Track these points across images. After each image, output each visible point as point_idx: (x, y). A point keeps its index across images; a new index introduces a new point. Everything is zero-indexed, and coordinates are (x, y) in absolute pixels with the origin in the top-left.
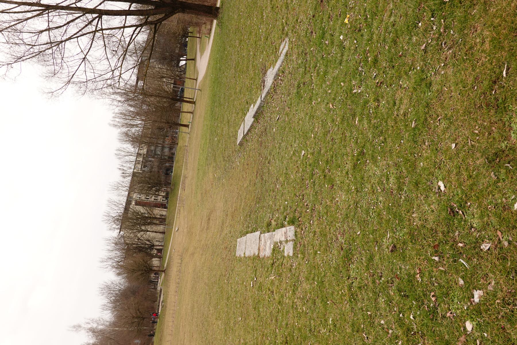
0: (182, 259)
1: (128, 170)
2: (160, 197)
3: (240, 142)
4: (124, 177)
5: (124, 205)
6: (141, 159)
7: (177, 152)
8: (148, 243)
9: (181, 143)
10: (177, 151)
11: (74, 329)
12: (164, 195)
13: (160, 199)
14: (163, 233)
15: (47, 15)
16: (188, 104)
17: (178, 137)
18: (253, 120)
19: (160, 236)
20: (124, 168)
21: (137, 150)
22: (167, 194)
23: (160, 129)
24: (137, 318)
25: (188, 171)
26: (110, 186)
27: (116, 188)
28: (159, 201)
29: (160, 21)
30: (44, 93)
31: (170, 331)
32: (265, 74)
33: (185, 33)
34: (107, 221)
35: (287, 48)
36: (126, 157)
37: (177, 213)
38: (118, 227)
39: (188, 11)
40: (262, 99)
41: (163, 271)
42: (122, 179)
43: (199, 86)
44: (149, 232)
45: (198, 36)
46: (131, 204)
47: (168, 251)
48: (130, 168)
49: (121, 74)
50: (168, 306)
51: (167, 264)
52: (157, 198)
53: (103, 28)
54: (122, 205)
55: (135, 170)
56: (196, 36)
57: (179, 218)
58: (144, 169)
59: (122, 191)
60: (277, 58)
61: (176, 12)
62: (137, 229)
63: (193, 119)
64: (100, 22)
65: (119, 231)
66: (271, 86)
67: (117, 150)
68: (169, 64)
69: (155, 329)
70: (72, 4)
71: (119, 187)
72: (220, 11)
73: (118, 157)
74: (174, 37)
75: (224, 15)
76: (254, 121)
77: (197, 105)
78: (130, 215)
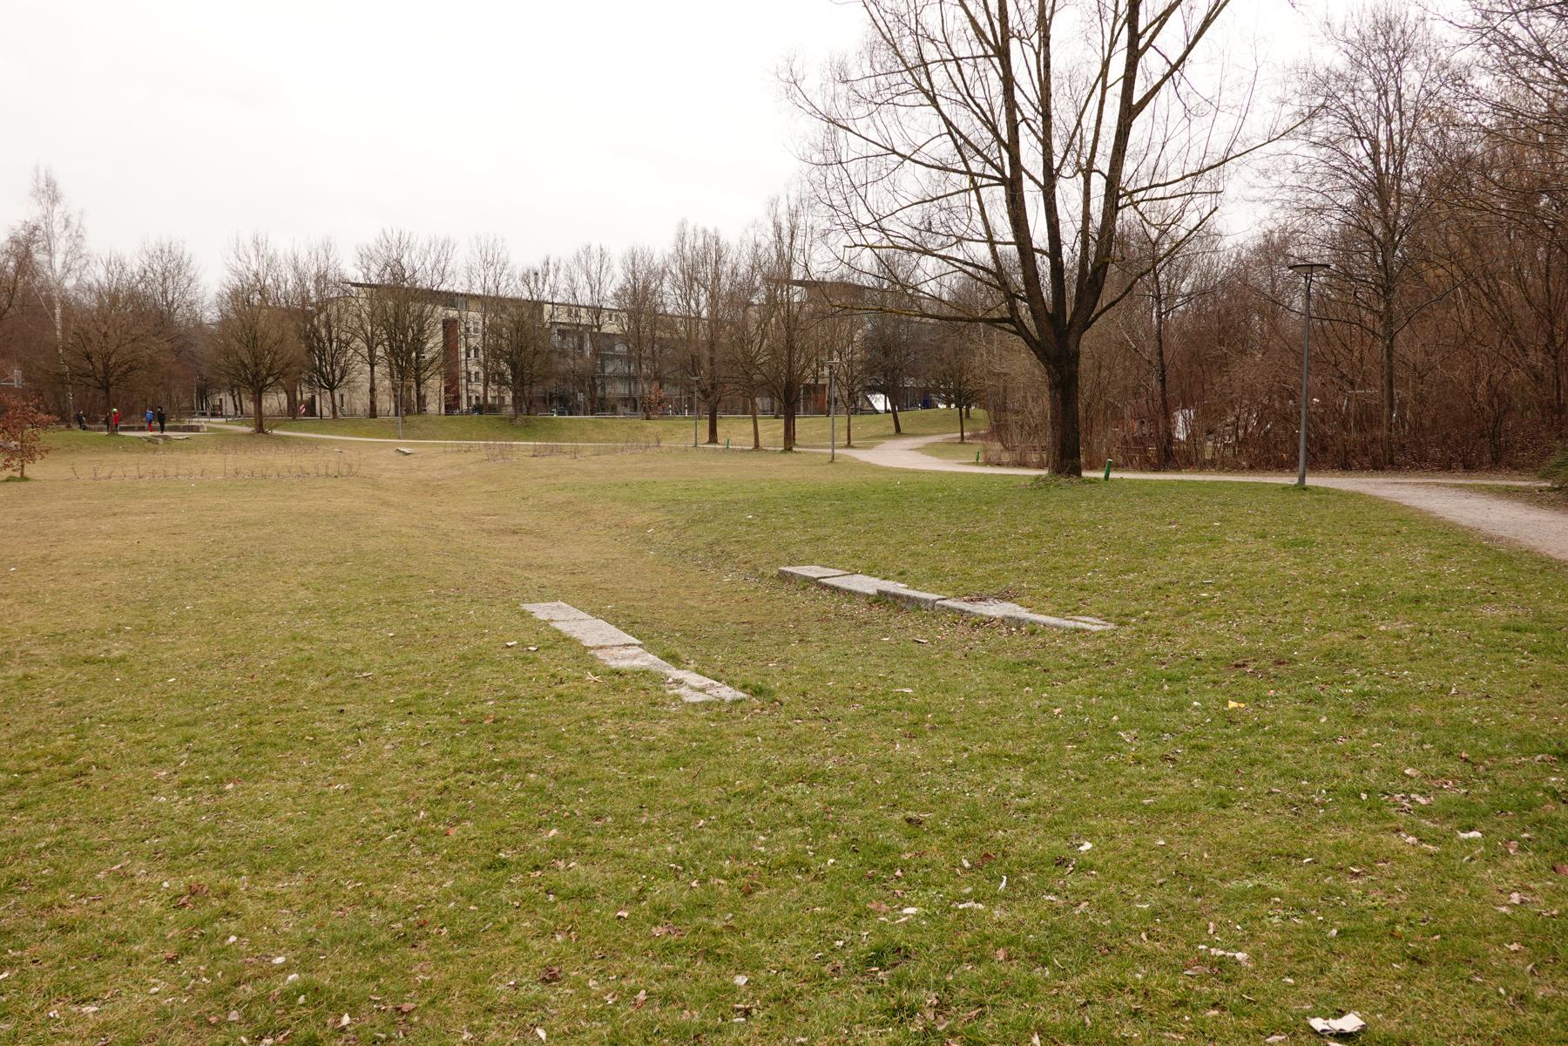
0: (342, 476)
3: (792, 574)
4: (525, 279)
5: (443, 288)
6: (585, 319)
7: (624, 421)
9: (655, 426)
10: (630, 421)
11: (42, 185)
12: (490, 400)
14: (373, 413)
15: (981, 52)
16: (782, 430)
17: (667, 419)
19: (361, 401)
22: (492, 409)
24: (106, 366)
25: (594, 458)
26: (491, 241)
27: (489, 259)
29: (1021, 330)
30: (790, 61)
31: (106, 474)
32: (1003, 599)
33: (968, 398)
34: (385, 243)
35: (1095, 628)
36: (585, 278)
37: (458, 445)
38: (373, 279)
39: (1058, 396)
40: (938, 602)
42: (518, 273)
43: (840, 455)
45: (965, 434)
47: (323, 434)
48: (554, 294)
49: (871, 247)
50: (160, 456)
51: (286, 436)
52: (473, 380)
53: (981, 190)
54: (439, 281)
55: (548, 308)
56: (965, 429)
59: (482, 277)
60: (1061, 611)
61: (1051, 367)
62: (372, 333)
63: (743, 451)
64: (996, 182)
65: (361, 280)
66: (981, 615)
67: (602, 249)
68: (870, 367)
69: (69, 427)
70: (1022, 115)
71: (492, 268)
72: (1074, 479)
73: (581, 253)
74: (952, 369)
75: (1067, 489)
76: (868, 596)
77: (960, 446)
78: (414, 307)
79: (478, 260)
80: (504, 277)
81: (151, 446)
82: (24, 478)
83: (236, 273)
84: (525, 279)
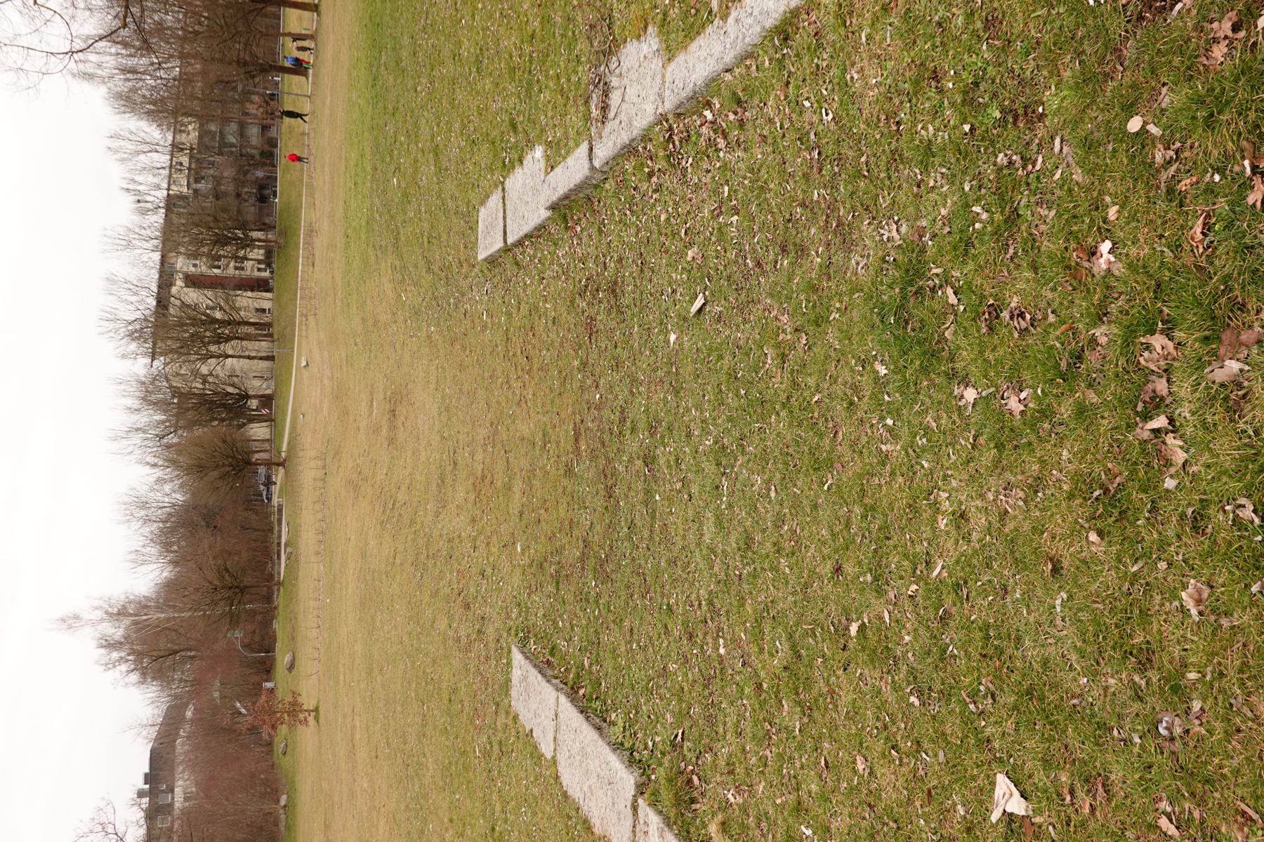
1: (153, 193)
2: (251, 263)
8: (230, 390)
13: (251, 270)
18: (544, 214)
20: (141, 188)
21: (170, 137)
23: (226, 84)
27: (124, 243)
28: (248, 273)
34: (112, 334)
36: (142, 157)
41: (279, 465)
42: (136, 218)
44: (230, 359)
46: (171, 284)
48: (158, 187)
57: (307, 337)
58: (194, 186)
71: (134, 242)
79: (125, 253)
80: (143, 232)
81: (293, 558)
82: (317, 710)
83: (147, 520)
84: (144, 212)
